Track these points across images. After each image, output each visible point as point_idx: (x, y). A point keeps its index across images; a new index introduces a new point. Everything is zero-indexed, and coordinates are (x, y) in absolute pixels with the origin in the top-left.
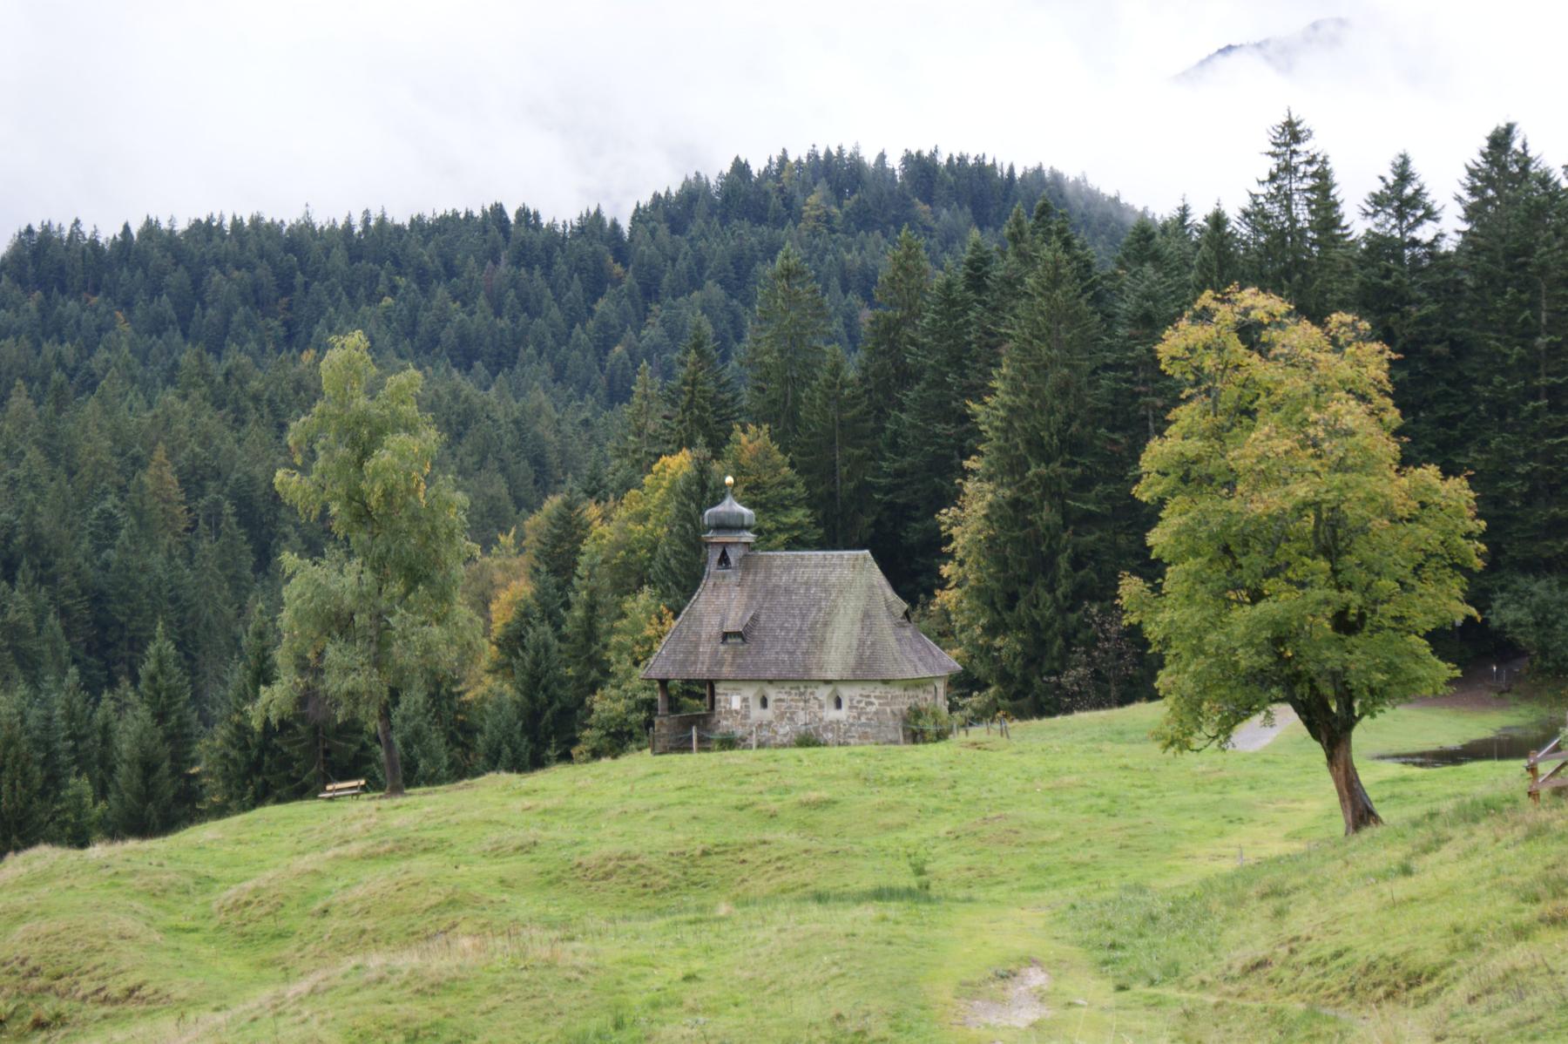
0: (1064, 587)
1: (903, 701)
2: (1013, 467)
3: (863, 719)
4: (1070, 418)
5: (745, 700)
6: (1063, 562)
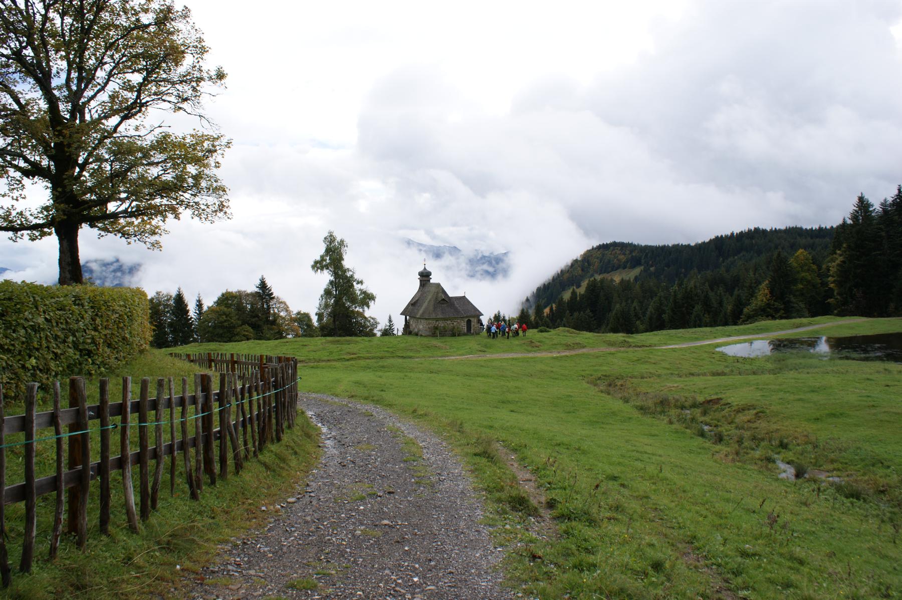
1: (434, 323)
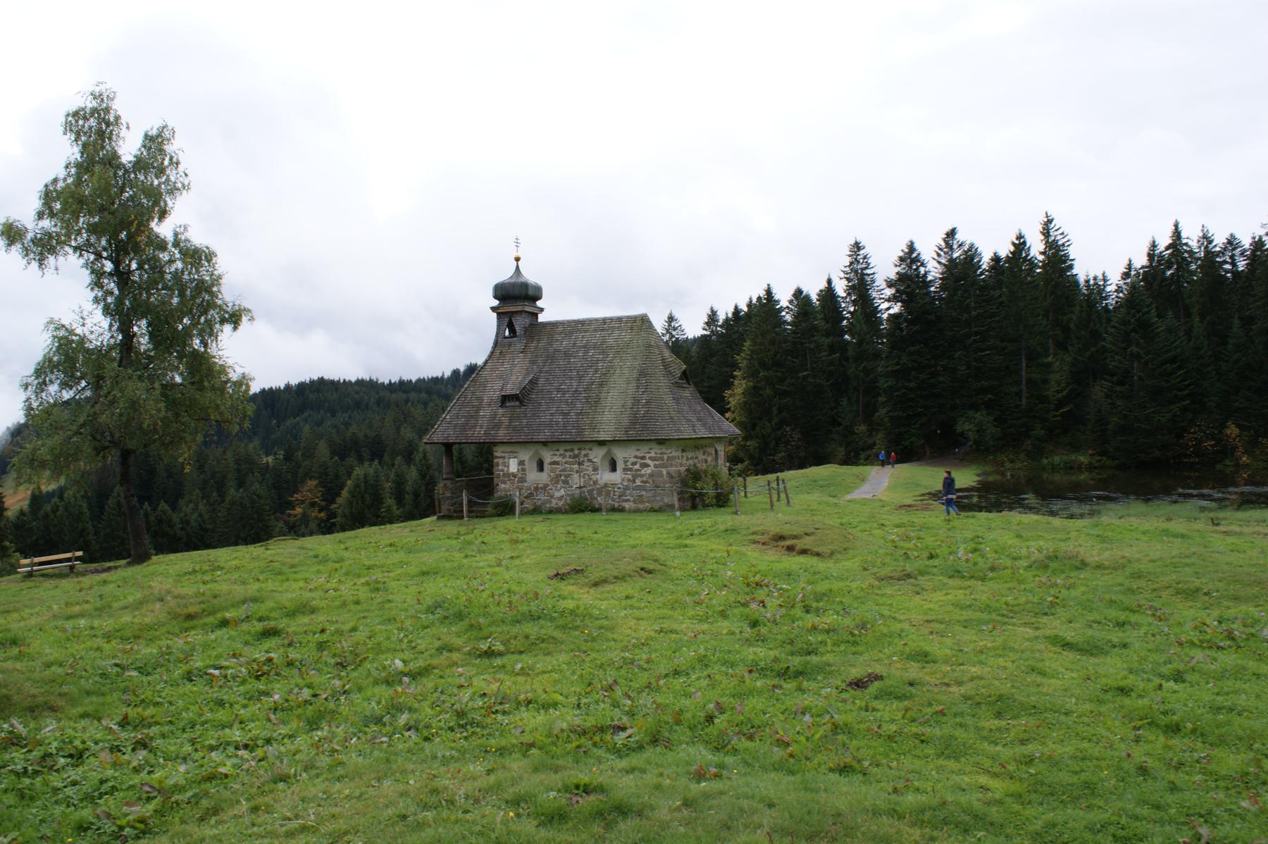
0: (775, 420)
1: (681, 462)
2: (752, 374)
3: (638, 483)
4: (776, 353)
5: (521, 463)
6: (775, 410)
